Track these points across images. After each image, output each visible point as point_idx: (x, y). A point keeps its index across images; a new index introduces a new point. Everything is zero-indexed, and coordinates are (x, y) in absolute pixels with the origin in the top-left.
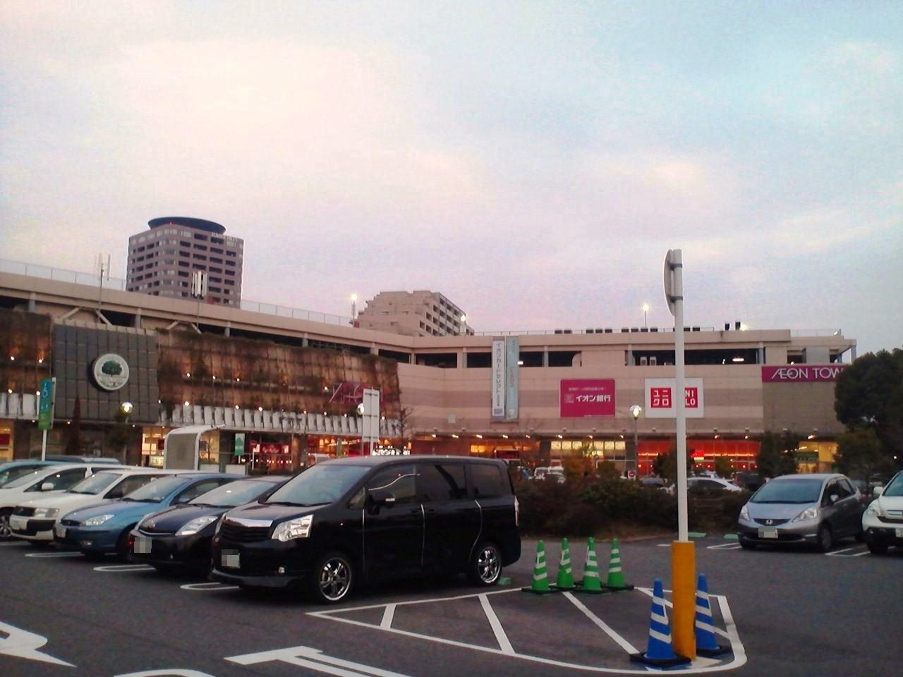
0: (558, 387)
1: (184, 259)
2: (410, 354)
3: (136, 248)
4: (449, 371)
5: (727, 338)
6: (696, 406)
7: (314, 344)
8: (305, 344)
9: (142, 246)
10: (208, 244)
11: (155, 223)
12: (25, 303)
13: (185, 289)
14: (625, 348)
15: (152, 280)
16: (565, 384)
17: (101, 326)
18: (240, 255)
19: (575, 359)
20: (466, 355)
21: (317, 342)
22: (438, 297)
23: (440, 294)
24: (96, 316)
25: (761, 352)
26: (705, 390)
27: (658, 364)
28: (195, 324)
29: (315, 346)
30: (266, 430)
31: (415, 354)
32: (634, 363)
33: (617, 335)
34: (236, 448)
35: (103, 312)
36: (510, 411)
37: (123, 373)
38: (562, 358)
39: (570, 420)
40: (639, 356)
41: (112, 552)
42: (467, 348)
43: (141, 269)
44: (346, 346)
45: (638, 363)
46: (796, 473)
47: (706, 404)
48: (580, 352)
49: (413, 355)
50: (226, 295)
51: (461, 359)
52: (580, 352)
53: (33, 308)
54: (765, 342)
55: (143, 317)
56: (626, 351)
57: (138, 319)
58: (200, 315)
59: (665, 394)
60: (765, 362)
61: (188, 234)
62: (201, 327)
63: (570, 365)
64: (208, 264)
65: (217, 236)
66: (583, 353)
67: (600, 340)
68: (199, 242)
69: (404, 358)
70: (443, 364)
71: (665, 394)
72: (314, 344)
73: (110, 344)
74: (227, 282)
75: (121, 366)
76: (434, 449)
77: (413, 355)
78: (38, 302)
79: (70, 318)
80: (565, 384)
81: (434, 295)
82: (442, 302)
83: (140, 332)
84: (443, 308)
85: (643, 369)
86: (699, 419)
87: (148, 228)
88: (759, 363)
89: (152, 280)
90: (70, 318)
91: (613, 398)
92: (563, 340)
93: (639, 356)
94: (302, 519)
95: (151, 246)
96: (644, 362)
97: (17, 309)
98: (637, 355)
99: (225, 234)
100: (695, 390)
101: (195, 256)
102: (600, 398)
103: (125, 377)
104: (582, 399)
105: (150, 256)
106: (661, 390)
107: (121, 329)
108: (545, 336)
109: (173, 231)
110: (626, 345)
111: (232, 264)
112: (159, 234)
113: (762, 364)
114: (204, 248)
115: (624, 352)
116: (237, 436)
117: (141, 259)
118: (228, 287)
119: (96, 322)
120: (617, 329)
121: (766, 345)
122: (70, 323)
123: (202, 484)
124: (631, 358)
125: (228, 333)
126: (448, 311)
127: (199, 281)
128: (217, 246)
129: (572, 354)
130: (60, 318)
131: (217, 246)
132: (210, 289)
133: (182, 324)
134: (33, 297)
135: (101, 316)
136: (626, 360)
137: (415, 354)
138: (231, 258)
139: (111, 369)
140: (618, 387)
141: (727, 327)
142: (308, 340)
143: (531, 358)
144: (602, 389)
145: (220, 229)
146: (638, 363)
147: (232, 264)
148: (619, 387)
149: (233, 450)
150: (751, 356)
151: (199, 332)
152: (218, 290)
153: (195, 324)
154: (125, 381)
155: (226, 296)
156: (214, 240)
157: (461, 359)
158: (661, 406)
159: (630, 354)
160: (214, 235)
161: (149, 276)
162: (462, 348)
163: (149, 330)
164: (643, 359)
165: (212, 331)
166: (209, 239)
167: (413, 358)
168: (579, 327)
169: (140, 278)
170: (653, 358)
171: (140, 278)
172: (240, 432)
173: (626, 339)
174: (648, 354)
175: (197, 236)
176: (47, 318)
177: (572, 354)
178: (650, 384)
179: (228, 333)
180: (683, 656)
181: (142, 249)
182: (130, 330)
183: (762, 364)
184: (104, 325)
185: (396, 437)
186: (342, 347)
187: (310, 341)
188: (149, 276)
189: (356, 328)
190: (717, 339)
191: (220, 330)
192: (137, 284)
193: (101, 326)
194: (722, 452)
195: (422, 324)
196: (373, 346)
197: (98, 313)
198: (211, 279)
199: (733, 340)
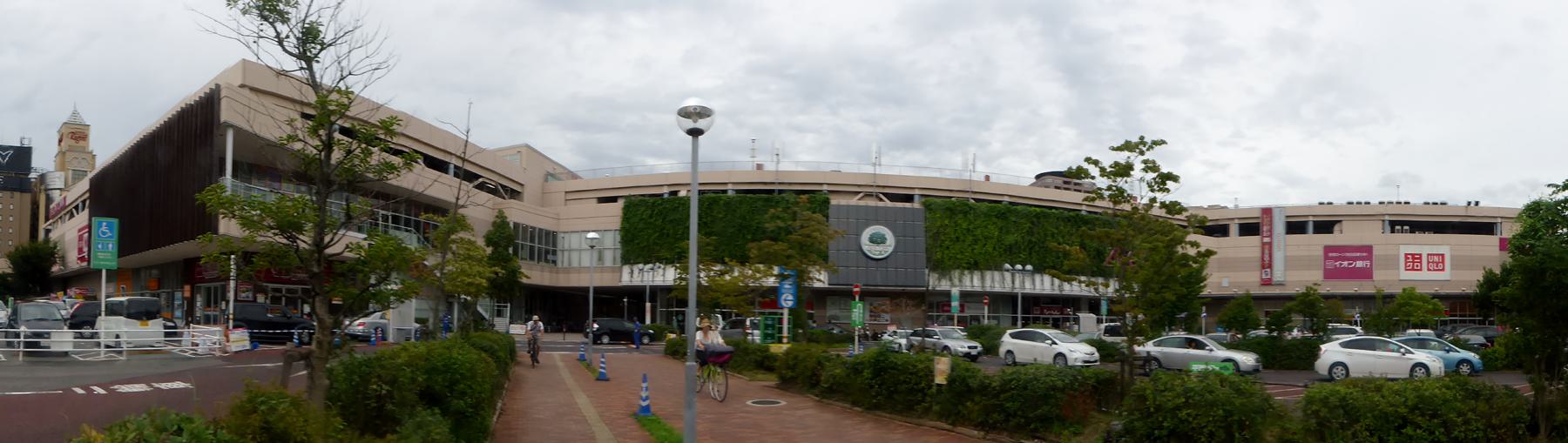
0: (1321, 252)
6: (1443, 270)
16: (1328, 249)
17: (881, 204)
19: (1336, 228)
20: (1237, 225)
25: (1499, 225)
26: (1398, 269)
27: (1411, 232)
30: (1037, 291)
33: (1374, 206)
37: (888, 242)
38: (1325, 227)
40: (1395, 225)
45: (1393, 231)
46: (699, 262)
51: (1234, 229)
54: (1502, 217)
59: (1417, 258)
63: (1332, 233)
67: (1361, 213)
68: (1066, 186)
71: (1417, 258)
73: (875, 217)
75: (887, 236)
80: (1328, 249)
85: (1398, 237)
87: (1035, 180)
91: (1371, 265)
93: (1395, 225)
96: (1398, 230)
98: (1393, 224)
100: (1443, 255)
102: (1359, 264)
103: (890, 246)
104: (1341, 264)
106: (1413, 255)
108: (1310, 207)
113: (1499, 236)
121: (1503, 220)
124: (1388, 228)
129: (1333, 223)
136: (1383, 229)
140: (1375, 252)
141: (1469, 203)
143: (1295, 227)
144: (1365, 254)
146: (1393, 231)
151: (1521, 385)
154: (890, 250)
156: (1076, 184)
157: (1234, 229)
158: (1413, 269)
162: (1233, 219)
164: (1398, 227)
170: (1406, 227)
173: (1382, 210)
174: (1402, 223)
175: (1065, 183)
177: (1333, 223)
178: (1404, 250)
183: (1499, 236)
185: (641, 266)
193: (881, 204)
199: (1476, 216)
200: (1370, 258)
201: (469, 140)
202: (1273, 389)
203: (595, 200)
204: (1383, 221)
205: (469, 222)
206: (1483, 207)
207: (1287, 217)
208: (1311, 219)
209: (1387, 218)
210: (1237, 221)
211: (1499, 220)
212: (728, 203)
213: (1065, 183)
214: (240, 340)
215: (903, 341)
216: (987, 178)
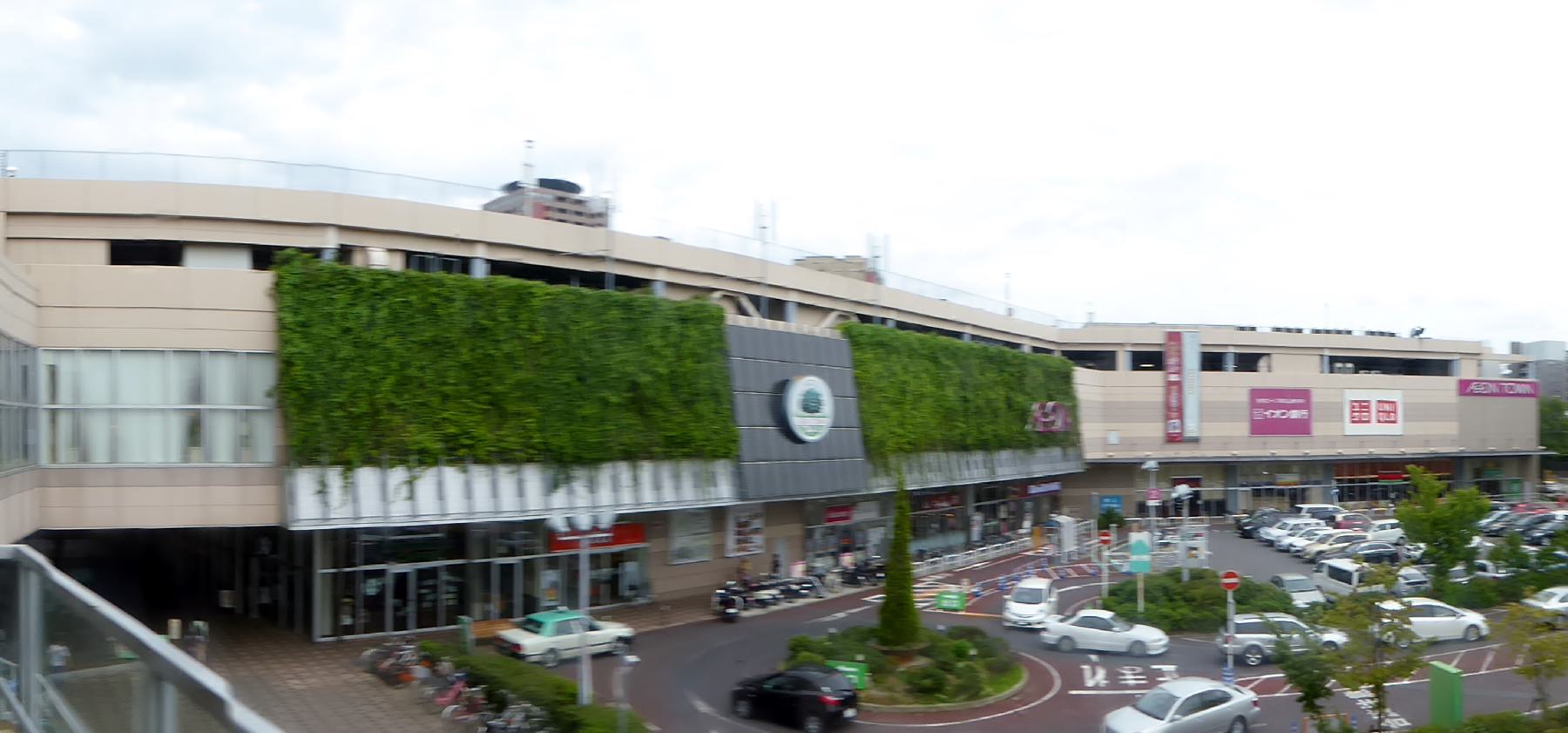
0: (1244, 397)
16: (1256, 393)
19: (1262, 363)
38: (1248, 362)
39: (1260, 439)
40: (1334, 362)
41: (918, 565)
47: (1407, 418)
51: (1123, 360)
53: (661, 293)
66: (1274, 357)
86: (1045, 483)
93: (1334, 362)
94: (1009, 553)
98: (1333, 360)
102: (1295, 414)
120: (1307, 327)
129: (1259, 356)
134: (661, 276)
143: (1212, 362)
148: (1316, 398)
157: (1123, 360)
164: (1339, 365)
167: (1230, 364)
168: (1265, 324)
173: (1321, 341)
180: (1481, 613)
182: (780, 325)
194: (1016, 713)
209: (1327, 353)
213: (561, 199)
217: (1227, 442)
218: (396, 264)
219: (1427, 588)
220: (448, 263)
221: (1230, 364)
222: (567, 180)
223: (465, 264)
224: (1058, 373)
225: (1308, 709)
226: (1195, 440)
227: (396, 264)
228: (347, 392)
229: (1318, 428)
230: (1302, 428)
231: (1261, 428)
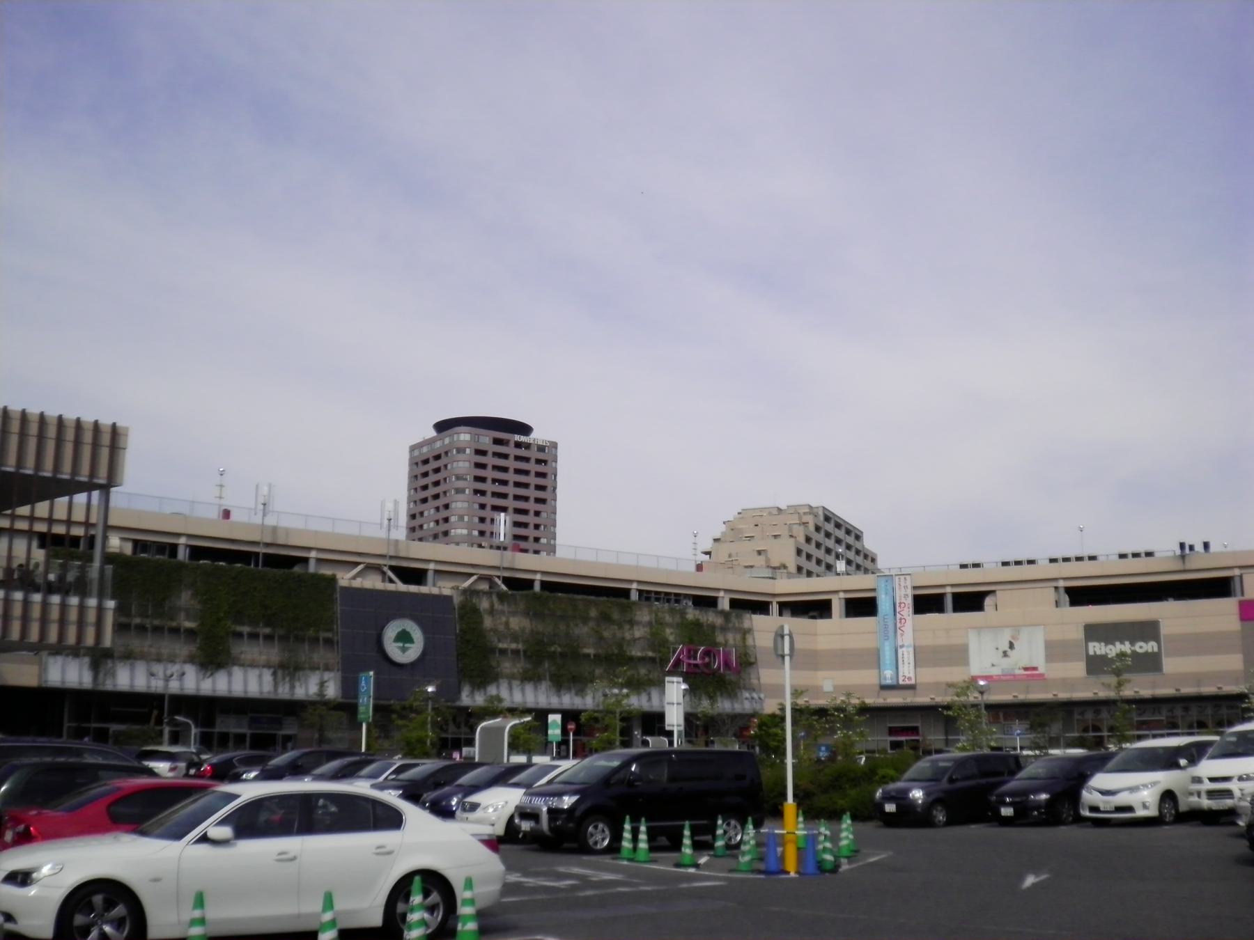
0: (1079, 634)
1: (480, 486)
2: (772, 602)
3: (419, 460)
4: (821, 623)
5: (1193, 563)
7: (645, 595)
8: (634, 596)
9: (425, 458)
10: (511, 450)
11: (443, 426)
12: (305, 560)
13: (483, 527)
14: (1055, 584)
15: (440, 502)
18: (554, 464)
19: (988, 601)
20: (843, 602)
21: (649, 592)
22: (821, 513)
23: (824, 508)
24: (384, 573)
25: (1237, 581)
28: (499, 577)
29: (648, 599)
31: (778, 603)
32: (1068, 603)
34: (550, 732)
35: (392, 568)
36: (886, 672)
42: (845, 591)
43: (425, 488)
44: (686, 596)
48: (993, 592)
49: (774, 604)
50: (536, 531)
51: (837, 607)
52: (993, 592)
55: (437, 572)
56: (1056, 588)
57: (430, 575)
58: (506, 565)
60: (1243, 594)
61: (486, 438)
62: (506, 581)
64: (510, 503)
65: (523, 439)
66: (997, 592)
69: (761, 607)
70: (814, 614)
72: (645, 595)
74: (538, 501)
76: (520, 836)
77: (774, 604)
78: (319, 561)
79: (354, 578)
81: (811, 510)
82: (827, 519)
83: (435, 591)
84: (830, 527)
87: (432, 433)
88: (1235, 596)
89: (440, 502)
90: (354, 578)
92: (971, 576)
95: (438, 457)
97: (297, 569)
99: (533, 435)
101: (494, 481)
105: (437, 470)
107: (413, 588)
109: (464, 436)
110: (1056, 579)
111: (542, 475)
112: (447, 441)
114: (505, 456)
115: (1053, 589)
116: (551, 718)
117: (425, 475)
118: (539, 507)
119: (383, 581)
120: (1042, 556)
121: (1243, 571)
122: (357, 583)
123: (459, 425)
125: (537, 587)
126: (836, 530)
127: (503, 524)
128: (522, 452)
130: (345, 578)
131: (522, 452)
132: (516, 537)
133: (482, 578)
135: (390, 574)
137: (778, 603)
138: (541, 468)
139: (404, 637)
142: (637, 590)
145: (525, 429)
147: (542, 475)
148: (1164, 630)
149: (546, 734)
150: (1218, 587)
151: (504, 587)
152: (525, 525)
153: (499, 577)
155: (537, 520)
156: (518, 445)
157: (837, 607)
159: (1062, 591)
160: (517, 438)
161: (436, 497)
163: (445, 588)
165: (518, 584)
166: (512, 444)
167: (775, 608)
169: (425, 500)
171: (425, 500)
172: (555, 711)
175: (497, 442)
176: (332, 580)
179: (537, 587)
181: (426, 462)
182: (424, 589)
184: (394, 585)
186: (682, 598)
187: (640, 592)
188: (436, 497)
189: (699, 573)
190: (1178, 566)
191: (529, 584)
192: (422, 507)
193: (391, 587)
195: (799, 552)
196: (721, 594)
197: (385, 569)
198: (517, 524)
199: (1201, 566)
200: (1157, 639)
201: (756, 644)
202: (719, 659)
203: (1049, 594)
204: (1056, 588)
205: (71, 657)
206: (1214, 553)
207: (915, 588)
208: (949, 590)
209: (1062, 584)
210: (842, 595)
211: (1237, 572)
212: (751, 610)
213: (497, 442)
214: (699, 862)
215: (1112, 748)
216: (227, 514)
217: (1065, 683)
218: (128, 549)
219: (826, 829)
220: (161, 548)
221: (775, 608)
222: (451, 417)
223: (174, 548)
224: (135, 659)
225: (121, 930)
226: (912, 687)
227: (128, 549)
228: (955, 690)
229: (1171, 665)
230: (1151, 663)
231: (1096, 665)
